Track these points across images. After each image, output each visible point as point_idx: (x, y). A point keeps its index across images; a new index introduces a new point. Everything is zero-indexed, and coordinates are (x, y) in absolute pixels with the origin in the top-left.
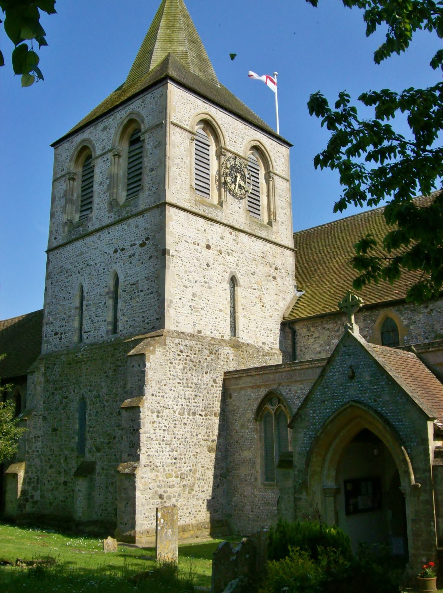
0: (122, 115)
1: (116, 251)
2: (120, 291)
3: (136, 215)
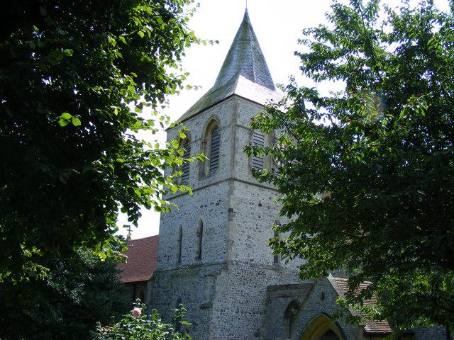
0: (207, 115)
1: (202, 207)
2: (204, 233)
3: (215, 184)
